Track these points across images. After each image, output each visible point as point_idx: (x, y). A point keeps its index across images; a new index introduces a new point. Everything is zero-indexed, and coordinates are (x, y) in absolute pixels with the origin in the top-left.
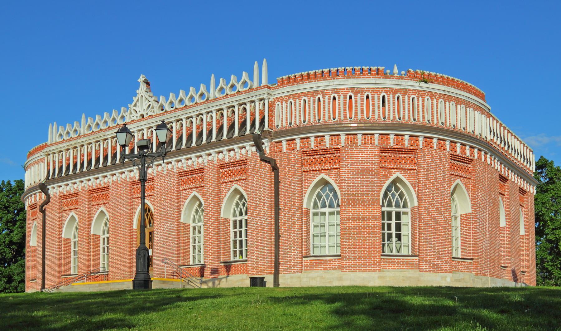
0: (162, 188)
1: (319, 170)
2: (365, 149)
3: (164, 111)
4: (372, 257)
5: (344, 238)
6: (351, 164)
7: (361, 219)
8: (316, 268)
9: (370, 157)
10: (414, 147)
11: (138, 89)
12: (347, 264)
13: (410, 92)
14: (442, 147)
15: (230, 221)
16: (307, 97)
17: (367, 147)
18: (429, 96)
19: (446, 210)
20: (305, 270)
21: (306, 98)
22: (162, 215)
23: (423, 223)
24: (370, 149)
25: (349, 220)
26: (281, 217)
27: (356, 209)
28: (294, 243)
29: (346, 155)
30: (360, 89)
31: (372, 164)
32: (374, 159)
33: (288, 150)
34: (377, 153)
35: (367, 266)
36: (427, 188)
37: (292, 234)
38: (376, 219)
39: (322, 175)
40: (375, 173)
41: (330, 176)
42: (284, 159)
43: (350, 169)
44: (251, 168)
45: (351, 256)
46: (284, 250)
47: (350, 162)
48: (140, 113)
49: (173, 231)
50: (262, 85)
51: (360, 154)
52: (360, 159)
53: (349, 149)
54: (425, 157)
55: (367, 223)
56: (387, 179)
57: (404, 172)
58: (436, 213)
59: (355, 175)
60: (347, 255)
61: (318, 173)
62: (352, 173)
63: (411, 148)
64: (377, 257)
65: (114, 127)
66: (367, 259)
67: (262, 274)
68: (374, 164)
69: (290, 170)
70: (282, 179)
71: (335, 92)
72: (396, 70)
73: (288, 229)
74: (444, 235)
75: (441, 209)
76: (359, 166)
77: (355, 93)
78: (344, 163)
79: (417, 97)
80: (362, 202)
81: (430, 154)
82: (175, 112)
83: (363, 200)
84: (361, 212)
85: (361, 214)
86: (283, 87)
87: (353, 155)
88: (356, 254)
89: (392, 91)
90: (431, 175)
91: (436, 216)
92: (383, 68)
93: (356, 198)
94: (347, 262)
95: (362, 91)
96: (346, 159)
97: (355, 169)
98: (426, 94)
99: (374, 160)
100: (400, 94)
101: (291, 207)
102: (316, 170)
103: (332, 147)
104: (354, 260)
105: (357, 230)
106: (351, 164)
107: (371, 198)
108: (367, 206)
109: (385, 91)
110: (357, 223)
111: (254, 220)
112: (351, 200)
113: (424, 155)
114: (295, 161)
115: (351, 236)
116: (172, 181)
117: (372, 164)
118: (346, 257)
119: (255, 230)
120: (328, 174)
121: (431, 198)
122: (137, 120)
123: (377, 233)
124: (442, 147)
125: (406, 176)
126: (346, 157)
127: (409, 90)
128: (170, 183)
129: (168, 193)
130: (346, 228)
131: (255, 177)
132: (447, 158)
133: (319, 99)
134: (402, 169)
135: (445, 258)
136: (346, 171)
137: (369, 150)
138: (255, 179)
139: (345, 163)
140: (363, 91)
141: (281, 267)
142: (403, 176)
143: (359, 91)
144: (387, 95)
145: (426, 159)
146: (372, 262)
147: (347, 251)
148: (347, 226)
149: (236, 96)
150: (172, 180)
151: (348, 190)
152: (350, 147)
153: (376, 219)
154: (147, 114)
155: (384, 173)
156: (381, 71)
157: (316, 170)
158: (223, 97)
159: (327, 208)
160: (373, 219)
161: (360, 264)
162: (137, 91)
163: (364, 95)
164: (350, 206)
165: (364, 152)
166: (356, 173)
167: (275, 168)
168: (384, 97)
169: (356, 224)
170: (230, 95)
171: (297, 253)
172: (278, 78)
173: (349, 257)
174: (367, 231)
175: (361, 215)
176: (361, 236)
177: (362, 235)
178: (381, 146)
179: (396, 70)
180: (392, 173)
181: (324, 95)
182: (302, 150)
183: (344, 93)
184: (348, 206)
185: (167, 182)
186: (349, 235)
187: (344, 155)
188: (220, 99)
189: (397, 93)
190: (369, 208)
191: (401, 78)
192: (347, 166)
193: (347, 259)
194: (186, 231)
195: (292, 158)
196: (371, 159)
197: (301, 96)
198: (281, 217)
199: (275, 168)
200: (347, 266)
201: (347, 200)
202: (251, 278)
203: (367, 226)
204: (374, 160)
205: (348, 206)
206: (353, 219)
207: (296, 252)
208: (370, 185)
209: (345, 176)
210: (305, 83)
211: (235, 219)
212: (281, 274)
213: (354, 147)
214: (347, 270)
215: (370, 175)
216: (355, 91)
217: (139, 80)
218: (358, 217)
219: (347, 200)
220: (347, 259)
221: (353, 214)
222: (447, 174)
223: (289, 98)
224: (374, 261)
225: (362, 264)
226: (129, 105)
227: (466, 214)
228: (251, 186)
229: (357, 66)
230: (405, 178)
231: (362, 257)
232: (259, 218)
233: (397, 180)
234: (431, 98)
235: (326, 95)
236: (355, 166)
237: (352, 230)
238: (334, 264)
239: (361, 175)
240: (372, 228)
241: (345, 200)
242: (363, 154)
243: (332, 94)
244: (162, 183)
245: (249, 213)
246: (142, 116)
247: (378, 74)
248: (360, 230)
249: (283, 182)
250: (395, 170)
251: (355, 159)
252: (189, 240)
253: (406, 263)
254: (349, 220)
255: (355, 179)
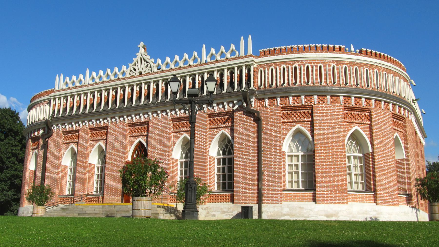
0: (157, 130)
1: (295, 122)
2: (333, 107)
3: (161, 70)
4: (341, 192)
5: (318, 176)
6: (322, 118)
7: (331, 161)
8: (293, 200)
9: (336, 113)
10: (368, 107)
11: (138, 52)
12: (321, 198)
13: (364, 66)
14: (387, 108)
15: (215, 158)
16: (286, 65)
17: (334, 105)
18: (377, 69)
19: (392, 156)
20: (284, 201)
21: (285, 66)
22: (156, 151)
23: (378, 166)
24: (336, 107)
25: (322, 162)
26: (263, 158)
27: (327, 154)
28: (275, 179)
29: (318, 111)
30: (327, 61)
31: (339, 119)
32: (340, 114)
33: (269, 105)
34: (341, 111)
35: (337, 199)
36: (379, 139)
37: (274, 171)
38: (343, 162)
39: (298, 126)
40: (341, 126)
41: (305, 127)
42: (266, 112)
43: (322, 122)
44: (238, 118)
45: (324, 191)
46: (266, 184)
47: (321, 117)
48: (139, 71)
49: (165, 165)
50: (247, 55)
51: (329, 111)
52: (329, 114)
53: (320, 106)
54: (376, 115)
55: (336, 164)
56: (349, 131)
57: (360, 126)
58: (386, 158)
59: (325, 127)
60: (321, 190)
61: (294, 124)
62: (323, 125)
63: (366, 107)
64: (344, 192)
65: (115, 80)
66: (337, 194)
67: (247, 203)
68: (340, 119)
69: (272, 120)
70: (264, 127)
71: (308, 63)
72: (353, 49)
73: (270, 167)
74: (392, 175)
75: (389, 155)
76: (328, 119)
77: (324, 64)
78: (316, 117)
79: (369, 69)
80: (331, 148)
81: (380, 112)
82: (170, 71)
83: (332, 147)
84: (331, 156)
85: (331, 157)
86: (265, 57)
87: (324, 111)
88: (328, 189)
89: (351, 64)
90: (381, 129)
91: (386, 161)
92: (344, 46)
93: (326, 145)
94: (321, 196)
95: (329, 63)
96: (318, 114)
97: (326, 122)
98: (374, 67)
99: (340, 116)
100: (357, 66)
101: (273, 150)
102: (292, 122)
103: (307, 104)
104: (327, 195)
105: (328, 170)
106: (322, 118)
107: (338, 145)
108: (335, 151)
109: (346, 63)
110: (328, 164)
111: (240, 159)
112: (323, 146)
113: (375, 113)
114: (276, 114)
115: (324, 175)
116: (165, 125)
117: (339, 119)
118: (320, 192)
119: (241, 167)
120: (303, 125)
121: (382, 146)
122: (136, 76)
123: (344, 173)
124: (387, 108)
125: (362, 129)
126: (318, 112)
127: (363, 63)
128: (164, 126)
129: (162, 134)
130: (320, 168)
131: (241, 125)
132: (390, 116)
133: (296, 68)
134: (359, 123)
135: (394, 194)
136: (318, 124)
137: (336, 108)
138: (241, 126)
139: (317, 117)
140: (330, 63)
141: (264, 198)
142: (361, 128)
143: (326, 63)
144: (348, 66)
145: (377, 116)
146: (341, 197)
147: (321, 187)
148: (320, 167)
149: (225, 61)
150: (166, 124)
151: (320, 138)
152: (321, 105)
153: (343, 162)
154: (145, 72)
155: (347, 126)
156: (343, 49)
157: (292, 122)
158: (213, 62)
159: (300, 151)
160: (340, 162)
161: (339, 198)
162: (137, 54)
163: (331, 66)
164: (322, 151)
165: (332, 109)
166: (326, 125)
167: (257, 120)
168: (345, 68)
169: (328, 166)
170: (219, 61)
171: (278, 187)
172: (260, 50)
173: (322, 192)
174: (336, 171)
175: (331, 159)
176: (332, 175)
177: (332, 174)
178: (345, 105)
179: (353, 49)
180: (352, 126)
181: (299, 64)
182: (281, 106)
183: (315, 63)
184: (320, 151)
185: (161, 125)
186: (322, 174)
187: (316, 111)
188: (211, 63)
189: (355, 66)
190: (337, 153)
191: (355, 54)
192: (319, 119)
193: (321, 193)
194: (175, 165)
195: (273, 111)
196: (338, 114)
197: (280, 64)
198: (263, 158)
199: (257, 120)
200: (321, 199)
201: (319, 146)
202: (242, 207)
203: (336, 167)
204: (340, 116)
205: (320, 151)
206: (325, 161)
207: (277, 186)
208: (337, 135)
209: (318, 127)
210: (284, 54)
211: (219, 157)
212: (264, 203)
213: (324, 105)
214: (321, 202)
215: (337, 127)
216: (324, 62)
217: (139, 46)
218: (329, 160)
219: (319, 146)
220: (321, 193)
221: (325, 157)
222: (391, 129)
223: (270, 66)
224: (342, 195)
225: (300, 197)
226: (129, 64)
227: (401, 159)
228: (238, 131)
229: (300, 45)
230: (362, 130)
231: (333, 192)
232: (245, 158)
233: (356, 130)
234: (378, 71)
235: (301, 64)
236: (325, 119)
237: (324, 170)
238: (309, 197)
239: (330, 127)
240: (340, 169)
241: (318, 146)
242: (331, 111)
243: (306, 64)
244: (156, 126)
245: (236, 154)
246: (141, 73)
247: (328, 50)
248: (330, 170)
249: (265, 130)
250: (354, 124)
251: (325, 114)
252: (177, 172)
253: (365, 198)
254: (322, 162)
255: (326, 130)
